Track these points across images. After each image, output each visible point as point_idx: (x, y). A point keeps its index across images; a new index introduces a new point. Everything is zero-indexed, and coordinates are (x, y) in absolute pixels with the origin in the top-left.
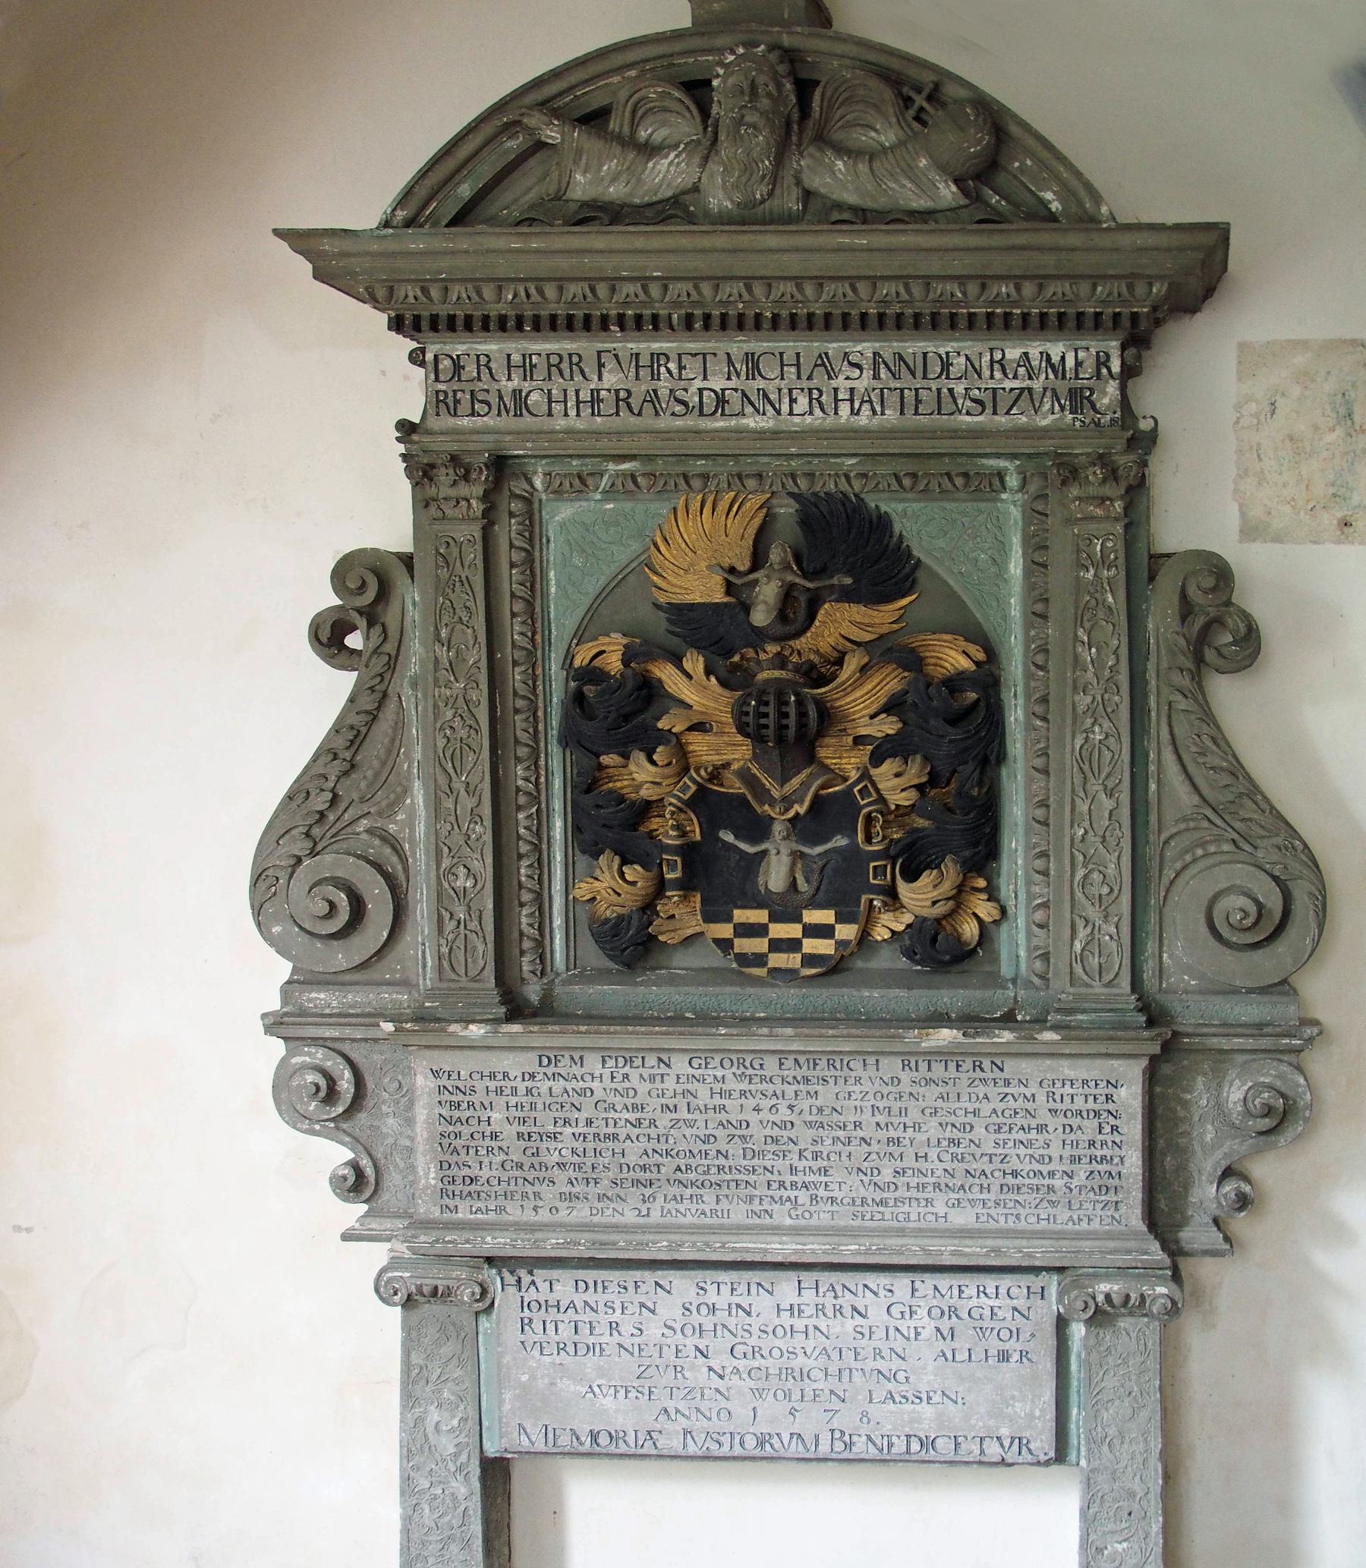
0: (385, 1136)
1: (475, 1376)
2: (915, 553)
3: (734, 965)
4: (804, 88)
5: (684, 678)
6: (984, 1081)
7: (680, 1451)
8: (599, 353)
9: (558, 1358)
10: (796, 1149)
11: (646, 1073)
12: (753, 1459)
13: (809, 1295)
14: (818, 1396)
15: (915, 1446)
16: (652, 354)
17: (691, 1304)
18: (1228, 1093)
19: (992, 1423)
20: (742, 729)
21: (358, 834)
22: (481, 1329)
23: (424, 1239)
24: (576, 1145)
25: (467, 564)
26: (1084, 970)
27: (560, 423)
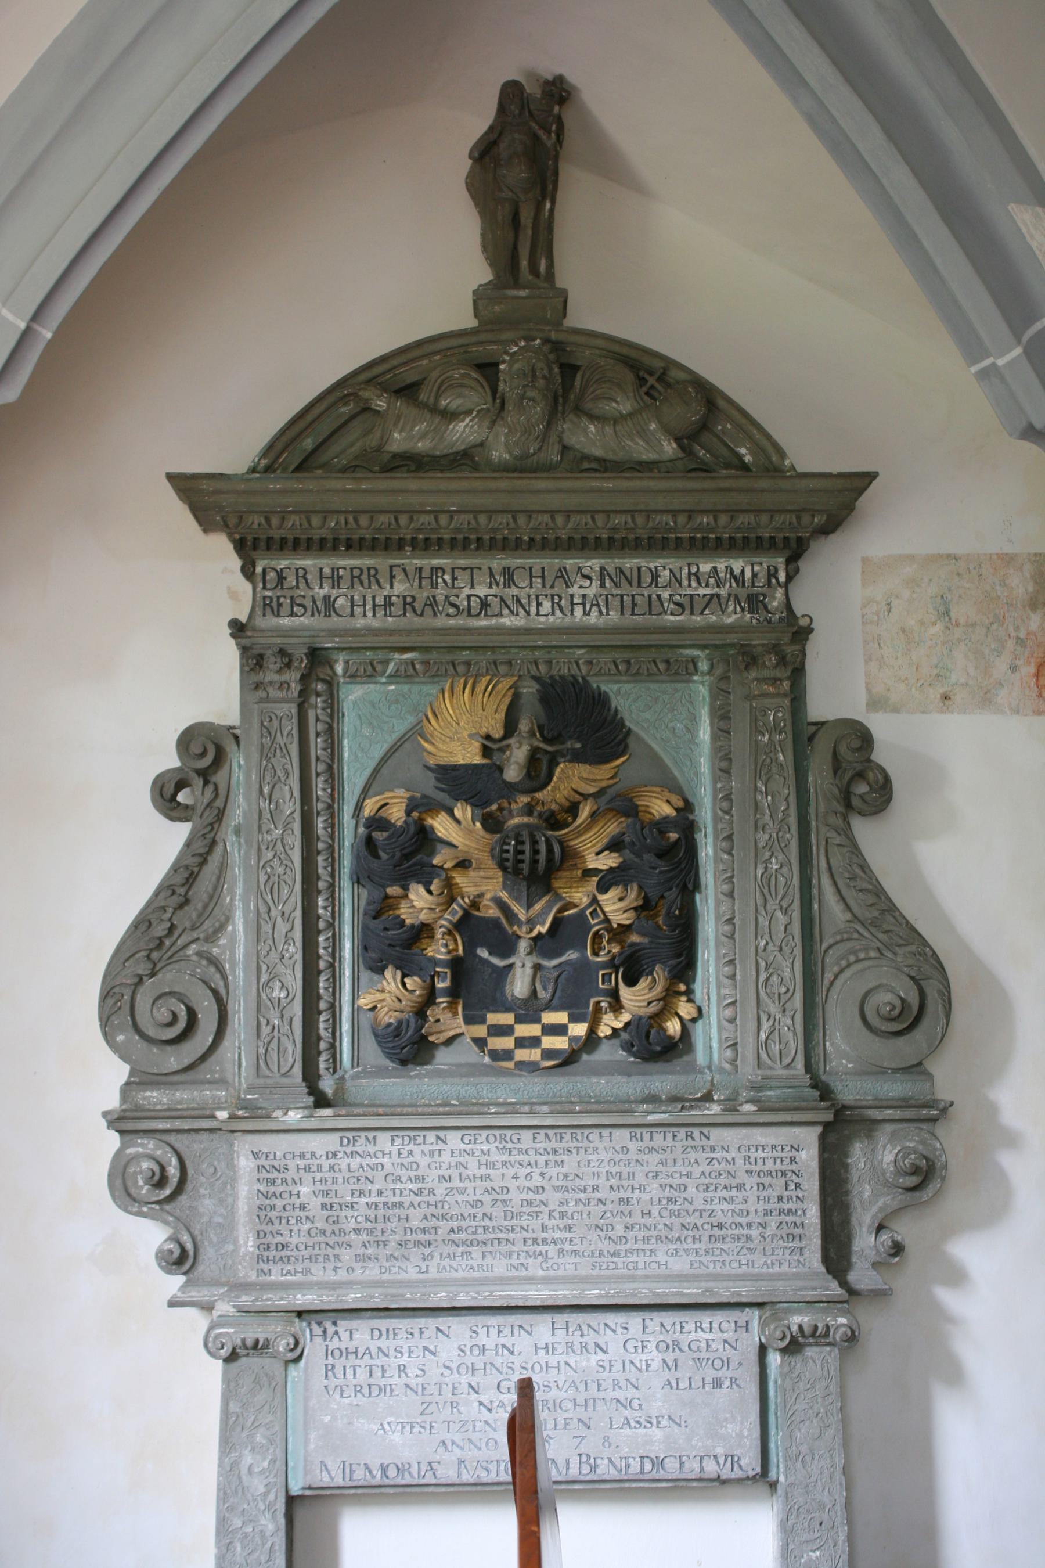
1: (283, 1421)
2: (628, 723)
3: (487, 1059)
5: (454, 824)
6: (694, 1148)
7: (455, 1480)
8: (391, 567)
10: (546, 1210)
11: (426, 1148)
15: (648, 1467)
16: (432, 569)
19: (709, 1443)
20: (502, 865)
22: (289, 1378)
25: (285, 734)
27: (360, 623)
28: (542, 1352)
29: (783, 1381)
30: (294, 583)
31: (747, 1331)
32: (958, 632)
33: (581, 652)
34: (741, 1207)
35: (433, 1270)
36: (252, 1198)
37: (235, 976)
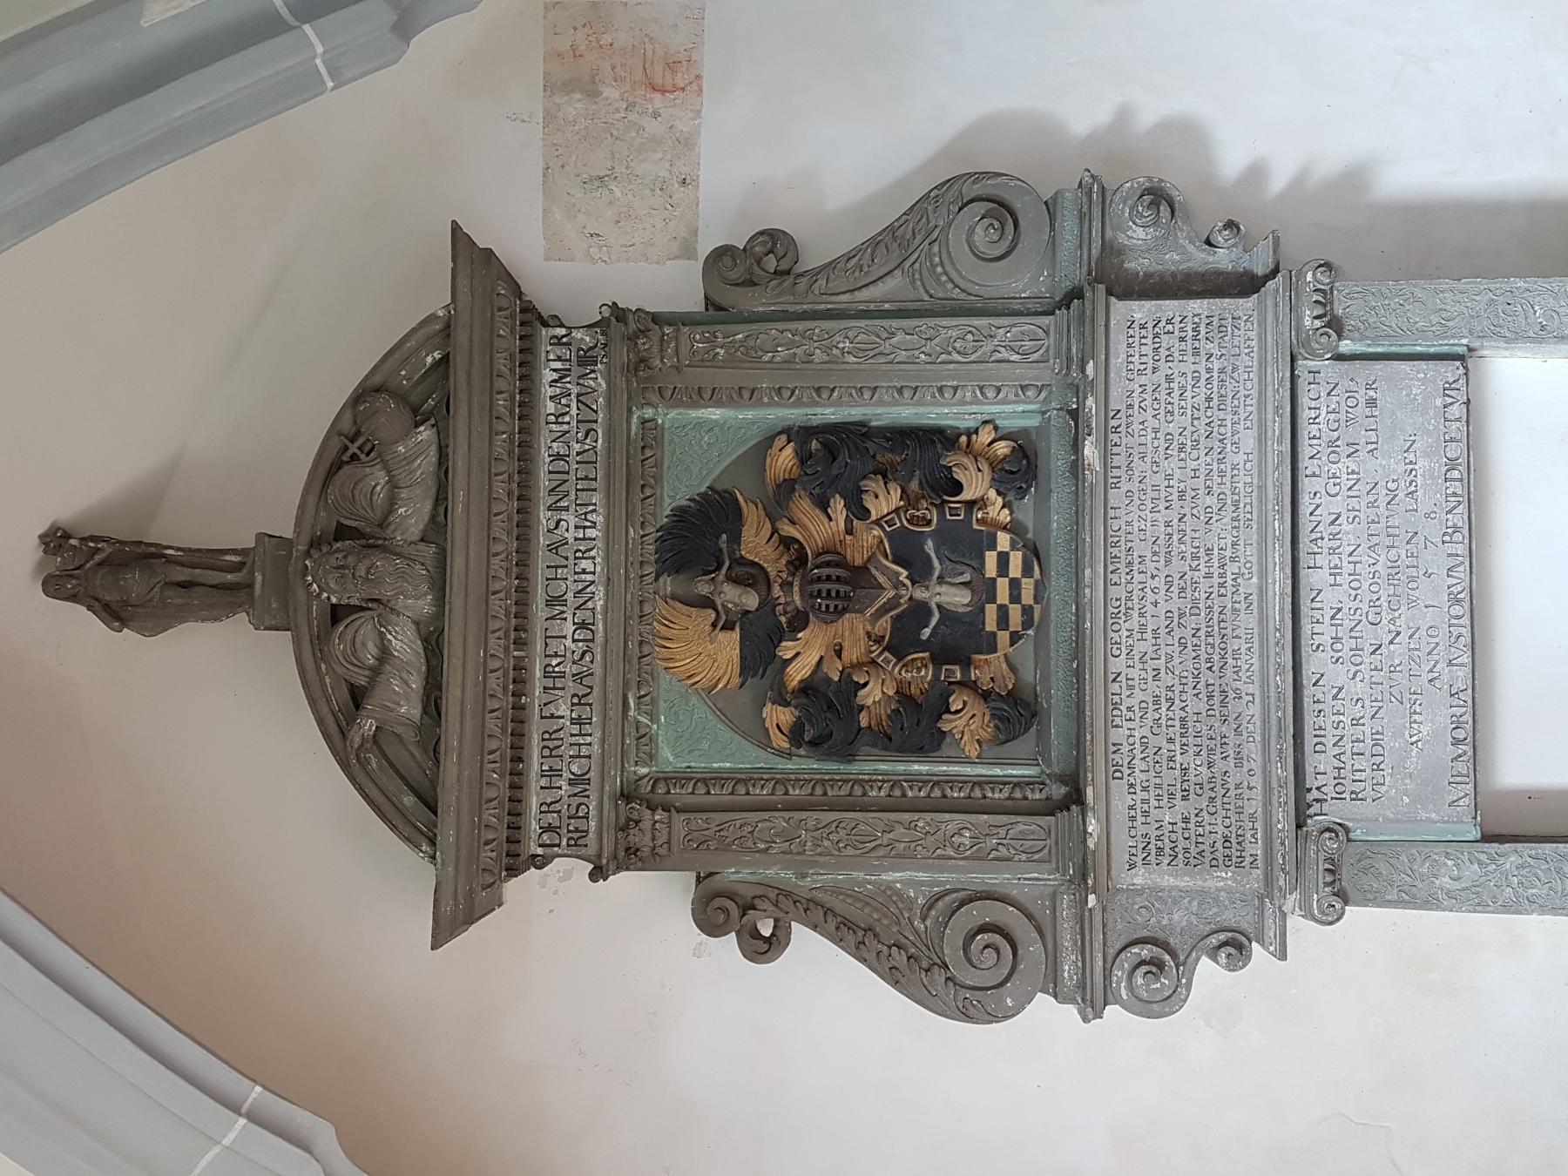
0: (1190, 923)
2: (703, 489)
3: (1031, 632)
4: (342, 533)
5: (799, 659)
7: (1468, 669)
8: (542, 718)
13: (1320, 560)
14: (1412, 553)
15: (1456, 474)
17: (1332, 657)
21: (926, 928)
24: (1191, 752)
30: (555, 815)
32: (620, 169)
34: (1189, 379)
35: (1251, 689)
36: (1177, 871)
37: (947, 882)
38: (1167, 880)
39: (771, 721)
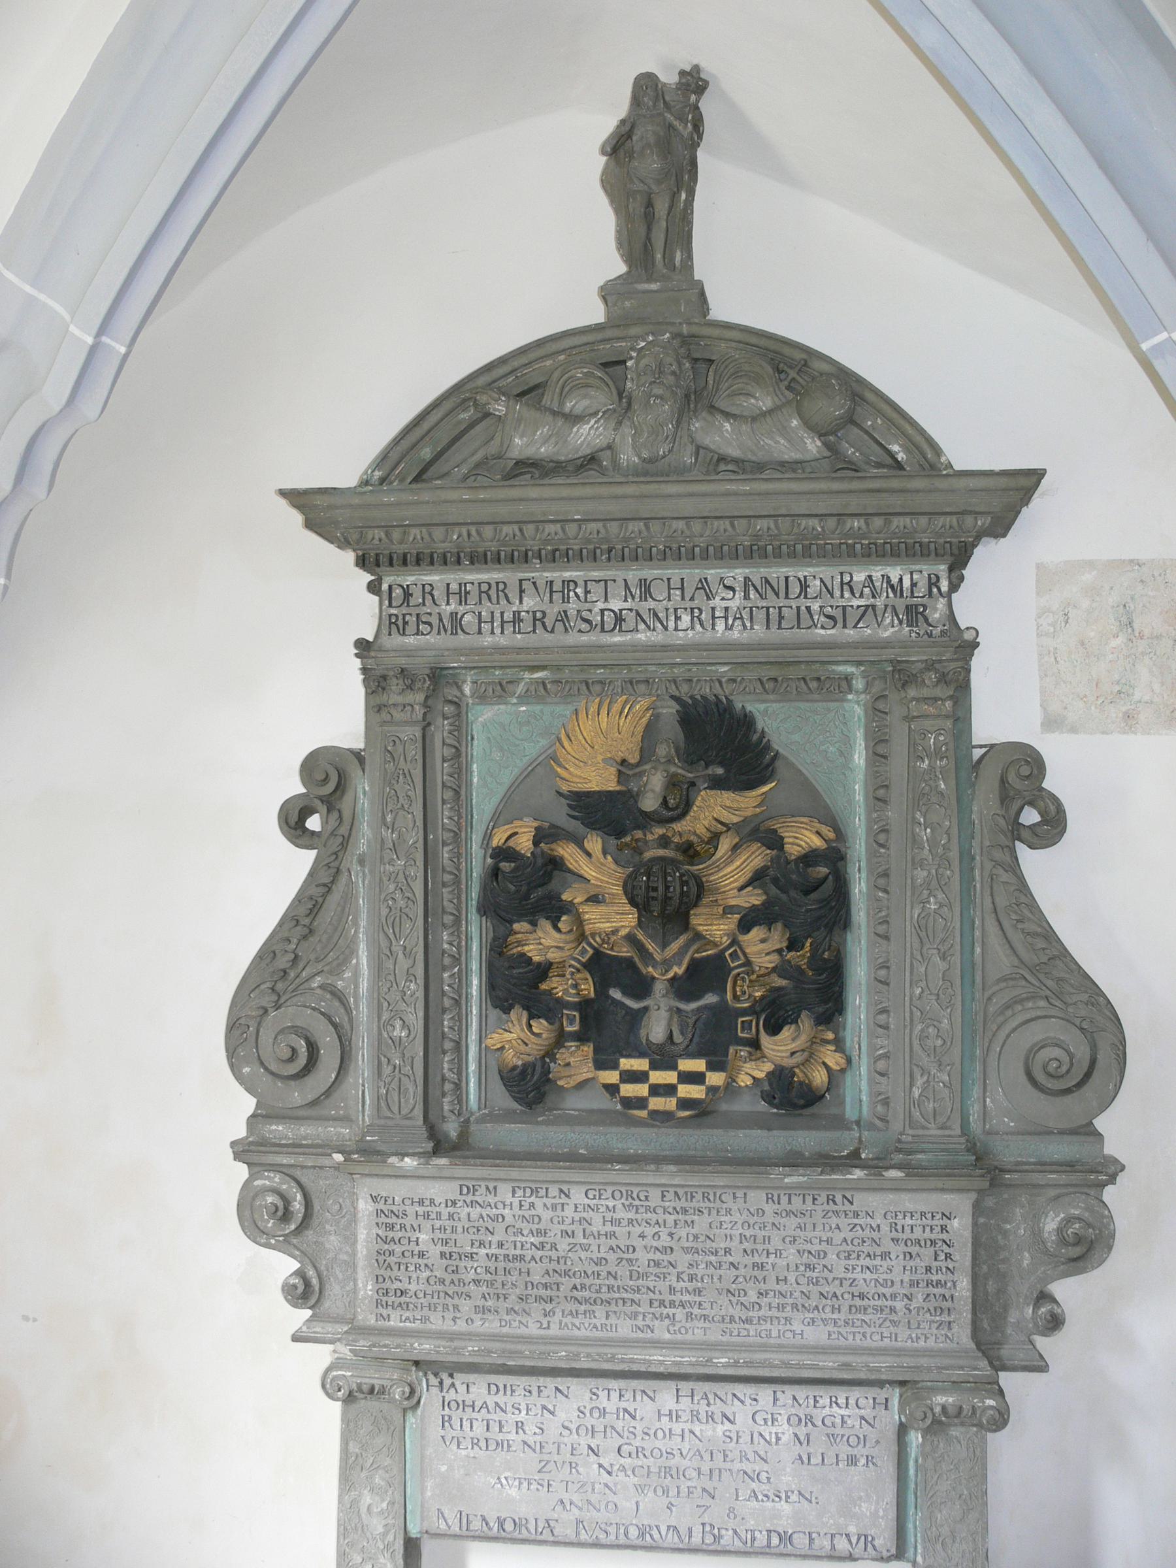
1: (402, 1465)
2: (776, 747)
3: (619, 1107)
5: (584, 856)
6: (836, 1213)
7: (573, 1538)
8: (521, 581)
9: (472, 1452)
11: (549, 1202)
12: (634, 1547)
13: (685, 1402)
14: (692, 1493)
15: (775, 1541)
17: (585, 1407)
18: (1044, 1224)
20: (632, 902)
21: (313, 989)
22: (408, 1424)
23: (363, 1344)
24: (489, 1264)
25: (409, 759)
26: (921, 1114)
27: (487, 640)
28: (665, 1419)
29: (924, 1460)
30: (421, 600)
31: (886, 1408)
33: (725, 669)
38: (364, 1234)
39: (521, 827)
